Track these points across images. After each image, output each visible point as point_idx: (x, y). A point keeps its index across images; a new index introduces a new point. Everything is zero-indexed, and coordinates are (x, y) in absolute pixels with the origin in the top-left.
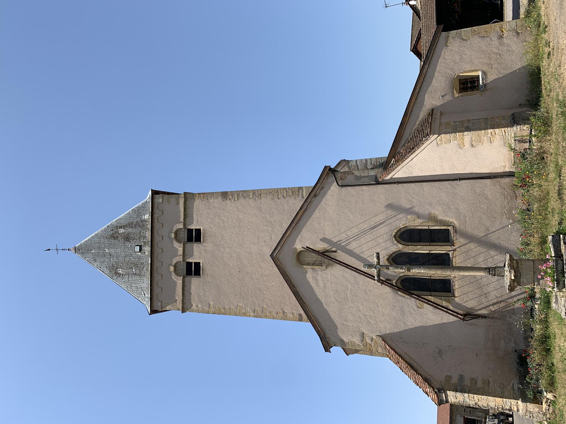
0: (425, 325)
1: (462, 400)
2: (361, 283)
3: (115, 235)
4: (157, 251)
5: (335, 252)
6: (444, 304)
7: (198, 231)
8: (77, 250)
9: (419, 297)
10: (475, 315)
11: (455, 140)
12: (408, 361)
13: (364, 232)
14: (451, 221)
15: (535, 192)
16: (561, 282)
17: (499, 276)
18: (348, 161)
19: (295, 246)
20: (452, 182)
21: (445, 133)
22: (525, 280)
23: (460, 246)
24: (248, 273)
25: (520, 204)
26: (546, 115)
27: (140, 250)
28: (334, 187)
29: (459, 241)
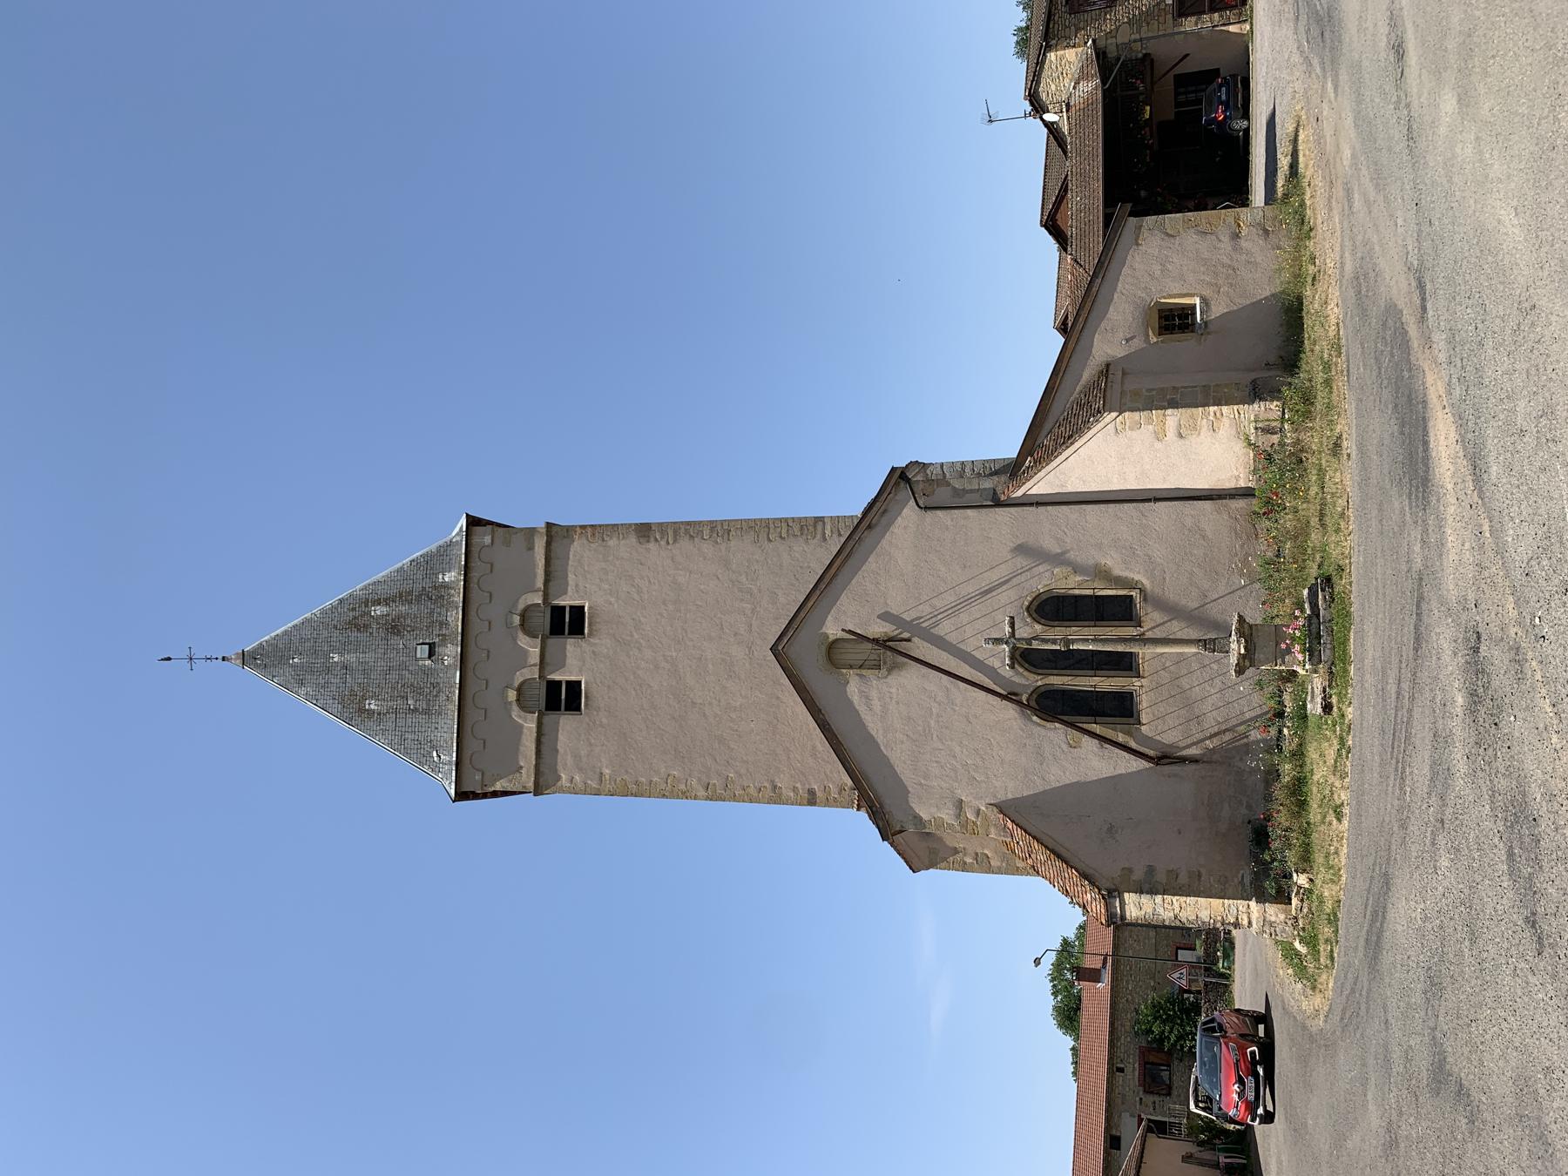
0: (1083, 779)
1: (1150, 911)
2: (958, 701)
3: (360, 622)
4: (475, 655)
5: (908, 640)
6: (1121, 738)
7: (578, 612)
8: (246, 658)
9: (1072, 725)
13: (967, 601)
15: (1288, 521)
21: (1132, 410)
25: (1264, 548)
27: (431, 654)
28: (910, 513)
29: (1151, 619)
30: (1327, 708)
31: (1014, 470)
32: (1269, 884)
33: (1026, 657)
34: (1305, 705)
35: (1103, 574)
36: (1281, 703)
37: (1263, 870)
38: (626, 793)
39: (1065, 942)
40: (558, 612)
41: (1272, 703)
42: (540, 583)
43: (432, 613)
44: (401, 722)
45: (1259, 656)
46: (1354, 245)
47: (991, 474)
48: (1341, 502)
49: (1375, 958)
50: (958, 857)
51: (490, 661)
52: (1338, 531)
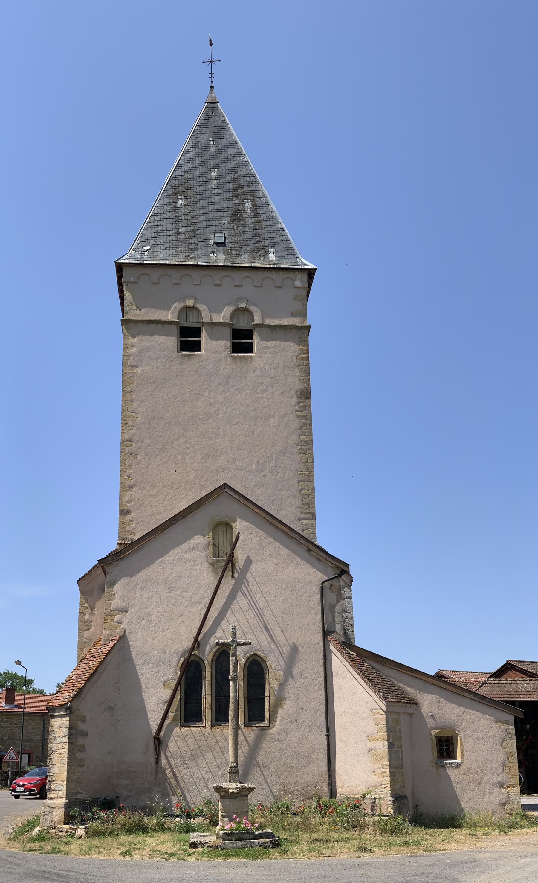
0: (143, 690)
1: (57, 734)
4: (218, 275)
5: (233, 577)
6: (171, 715)
7: (249, 349)
8: (212, 104)
10: (159, 751)
11: (378, 730)
12: (99, 669)
13: (260, 615)
14: (276, 723)
15: (315, 819)
16: (230, 838)
17: (230, 777)
18: (350, 586)
19: (239, 520)
20: (324, 726)
21: (387, 720)
22: (228, 803)
23: (244, 735)
24: (186, 430)
25: (297, 804)
26: (404, 831)
27: (218, 244)
28: (318, 577)
29: (250, 733)
30: (194, 845)
31: (347, 644)
32: (78, 810)
33: (223, 653)
34: (195, 831)
35: (279, 702)
36: (196, 816)
37: (86, 806)
38: (125, 384)
39: (30, 682)
40: (249, 334)
41: (196, 810)
42: (268, 321)
43: (246, 244)
44: (170, 222)
45: (228, 801)
46: (496, 859)
47: (344, 630)
48: (328, 853)
49: (34, 876)
50: (89, 610)
51: (212, 278)
52: (310, 850)
